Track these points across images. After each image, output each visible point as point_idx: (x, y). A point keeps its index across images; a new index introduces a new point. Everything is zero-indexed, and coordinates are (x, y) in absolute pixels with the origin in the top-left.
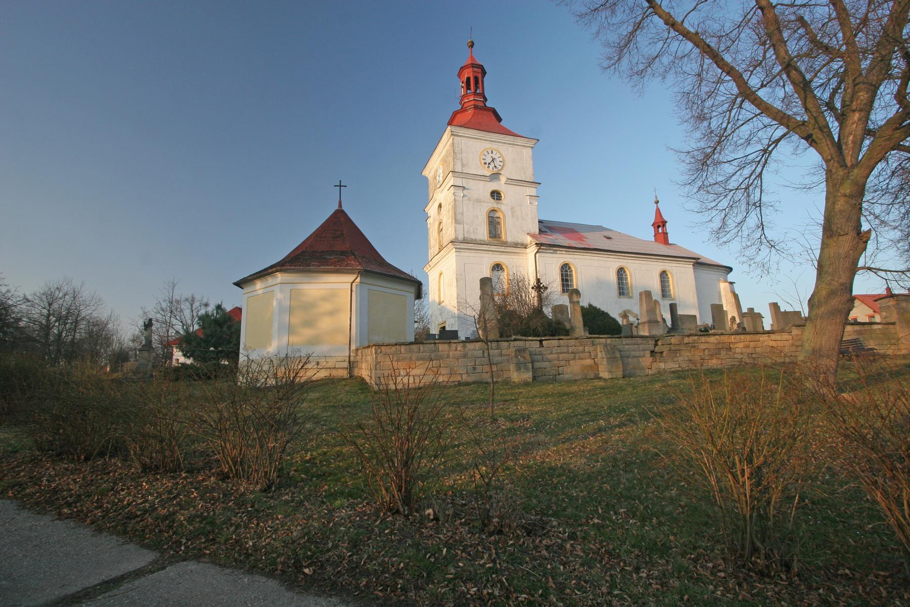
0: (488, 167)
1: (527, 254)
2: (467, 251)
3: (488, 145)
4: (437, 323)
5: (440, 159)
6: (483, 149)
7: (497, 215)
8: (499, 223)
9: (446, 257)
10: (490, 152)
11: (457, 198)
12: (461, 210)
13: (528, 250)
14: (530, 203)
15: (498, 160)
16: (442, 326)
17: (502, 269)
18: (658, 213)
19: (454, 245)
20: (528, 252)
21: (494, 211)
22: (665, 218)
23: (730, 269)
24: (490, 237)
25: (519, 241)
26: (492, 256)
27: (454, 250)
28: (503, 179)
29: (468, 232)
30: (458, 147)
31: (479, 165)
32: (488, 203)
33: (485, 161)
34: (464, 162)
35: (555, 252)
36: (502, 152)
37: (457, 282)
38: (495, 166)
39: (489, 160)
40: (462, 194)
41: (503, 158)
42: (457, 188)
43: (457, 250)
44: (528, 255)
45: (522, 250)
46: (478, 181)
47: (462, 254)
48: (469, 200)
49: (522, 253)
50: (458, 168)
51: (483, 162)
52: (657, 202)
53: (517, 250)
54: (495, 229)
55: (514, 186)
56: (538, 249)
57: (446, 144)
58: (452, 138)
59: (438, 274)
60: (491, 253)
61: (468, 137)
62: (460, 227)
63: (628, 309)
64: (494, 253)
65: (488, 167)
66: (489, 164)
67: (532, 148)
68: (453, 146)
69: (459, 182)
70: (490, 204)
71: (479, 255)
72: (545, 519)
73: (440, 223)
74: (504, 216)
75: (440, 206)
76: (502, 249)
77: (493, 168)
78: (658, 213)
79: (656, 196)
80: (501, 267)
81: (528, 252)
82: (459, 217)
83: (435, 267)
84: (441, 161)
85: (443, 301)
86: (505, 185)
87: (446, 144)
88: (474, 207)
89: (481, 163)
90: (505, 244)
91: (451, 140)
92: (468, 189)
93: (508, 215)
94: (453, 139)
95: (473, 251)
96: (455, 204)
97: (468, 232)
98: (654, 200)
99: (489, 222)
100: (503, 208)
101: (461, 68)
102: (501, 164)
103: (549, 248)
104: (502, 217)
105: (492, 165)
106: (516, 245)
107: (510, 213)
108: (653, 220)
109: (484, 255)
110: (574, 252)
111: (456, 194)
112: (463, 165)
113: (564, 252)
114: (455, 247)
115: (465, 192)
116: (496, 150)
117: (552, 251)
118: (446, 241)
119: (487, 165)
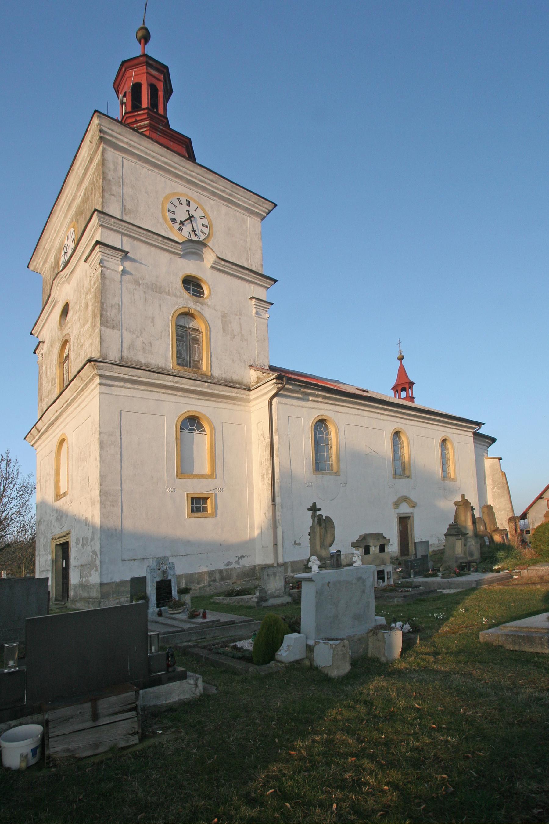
0: (180, 229)
1: (249, 401)
2: (129, 385)
3: (181, 188)
4: (50, 537)
5: (68, 220)
6: (168, 191)
7: (193, 324)
8: (196, 341)
9: (75, 405)
10: (184, 202)
11: (108, 273)
12: (116, 300)
13: (253, 394)
14: (257, 313)
15: (200, 222)
16: (61, 541)
17: (200, 427)
18: (402, 371)
19: (98, 368)
20: (252, 397)
21: (187, 314)
22: (412, 378)
23: (493, 440)
24: (178, 364)
25: (235, 378)
26: (182, 400)
27: (97, 380)
28: (209, 258)
29: (132, 346)
30: (115, 170)
31: (161, 220)
32: (176, 296)
33: (173, 216)
34: (128, 205)
35: (305, 397)
36: (207, 209)
37: (101, 448)
38: (194, 231)
39: (181, 216)
40: (121, 268)
41: (210, 221)
42: (110, 252)
43: (104, 381)
44: (252, 404)
45: (241, 394)
46: (158, 251)
47: (116, 391)
48: (137, 282)
49: (241, 400)
50: (114, 210)
51: (169, 216)
52: (401, 359)
53: (233, 393)
54: (189, 350)
55: (229, 278)
56: (280, 389)
57: (85, 174)
58: (101, 149)
59: (55, 441)
60: (179, 393)
61: (140, 158)
62: (113, 335)
63: (405, 494)
64: (186, 395)
65: (180, 229)
66: (182, 223)
67: (263, 218)
68: (103, 164)
69: (114, 240)
70: (180, 300)
71: (156, 396)
72: (118, 600)
73: (66, 342)
74: (209, 329)
75: (65, 311)
76: (204, 388)
77: (189, 234)
78: (402, 371)
79: (400, 351)
80: (199, 423)
81: (252, 397)
82: (112, 313)
83: (50, 431)
84: (72, 221)
85: (65, 494)
86: (211, 271)
87: (85, 174)
88: (146, 300)
89: (164, 218)
90: (208, 379)
91: (98, 158)
92: (134, 261)
93: (217, 325)
94: (104, 150)
95: (142, 387)
96: (103, 284)
97: (132, 346)
98: (397, 355)
99: (177, 335)
100: (207, 313)
101: (123, 63)
102: (206, 231)
103: (297, 388)
104: (203, 328)
105: (187, 228)
106: (229, 384)
107: (219, 323)
108: (393, 382)
109: (163, 397)
110: (335, 400)
111: (106, 264)
112: (124, 209)
113: (320, 399)
114: (101, 372)
115: (128, 265)
116: (196, 202)
117: (300, 396)
118: (74, 365)
119: (177, 226)
